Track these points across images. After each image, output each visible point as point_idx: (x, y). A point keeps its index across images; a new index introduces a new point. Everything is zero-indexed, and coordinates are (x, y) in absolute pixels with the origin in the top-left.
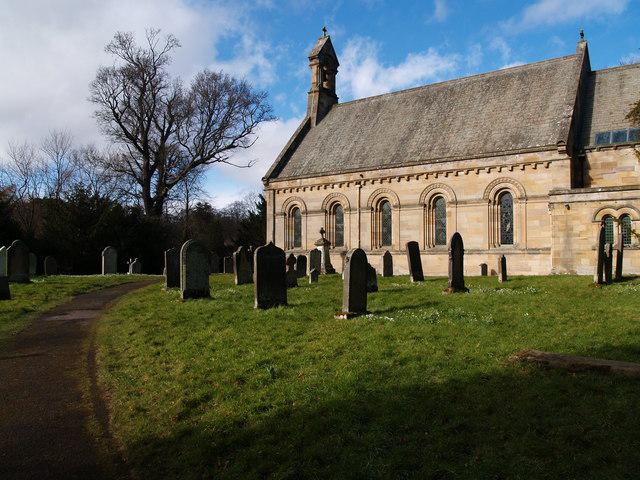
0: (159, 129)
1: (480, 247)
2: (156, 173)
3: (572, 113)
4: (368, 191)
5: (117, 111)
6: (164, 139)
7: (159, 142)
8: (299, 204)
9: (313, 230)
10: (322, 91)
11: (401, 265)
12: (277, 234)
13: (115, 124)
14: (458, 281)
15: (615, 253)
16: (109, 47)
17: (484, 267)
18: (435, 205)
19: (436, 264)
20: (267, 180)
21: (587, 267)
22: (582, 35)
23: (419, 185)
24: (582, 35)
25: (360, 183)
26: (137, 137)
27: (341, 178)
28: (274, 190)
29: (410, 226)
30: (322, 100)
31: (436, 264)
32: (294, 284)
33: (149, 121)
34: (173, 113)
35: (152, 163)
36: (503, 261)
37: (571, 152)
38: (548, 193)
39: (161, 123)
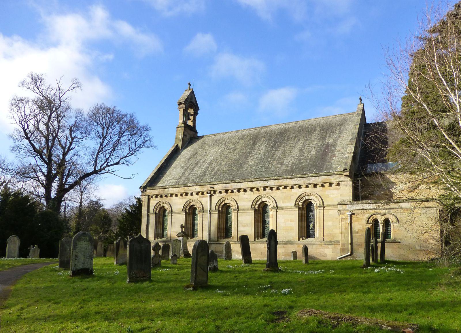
0: (62, 147)
1: (291, 239)
2: (56, 179)
3: (353, 150)
4: (216, 198)
5: (27, 131)
6: (65, 154)
7: (61, 157)
8: (166, 206)
9: (175, 226)
10: (186, 127)
11: (237, 254)
12: (148, 230)
13: (26, 142)
14: (272, 262)
15: (379, 245)
16: (23, 83)
17: (295, 254)
18: (261, 211)
19: (259, 251)
20: (144, 189)
21: (360, 255)
22: (361, 99)
23: (251, 196)
24: (361, 99)
25: (210, 193)
26: (45, 153)
27: (198, 189)
28: (149, 196)
29: (244, 224)
30: (186, 133)
31: (259, 251)
32: (158, 265)
33: (54, 140)
34: (73, 136)
35: (54, 172)
36: (306, 249)
37: (353, 176)
38: (337, 203)
39: (63, 141)
